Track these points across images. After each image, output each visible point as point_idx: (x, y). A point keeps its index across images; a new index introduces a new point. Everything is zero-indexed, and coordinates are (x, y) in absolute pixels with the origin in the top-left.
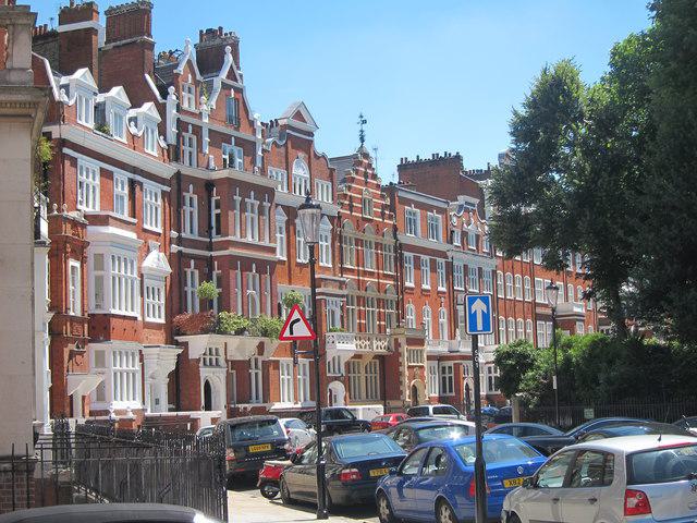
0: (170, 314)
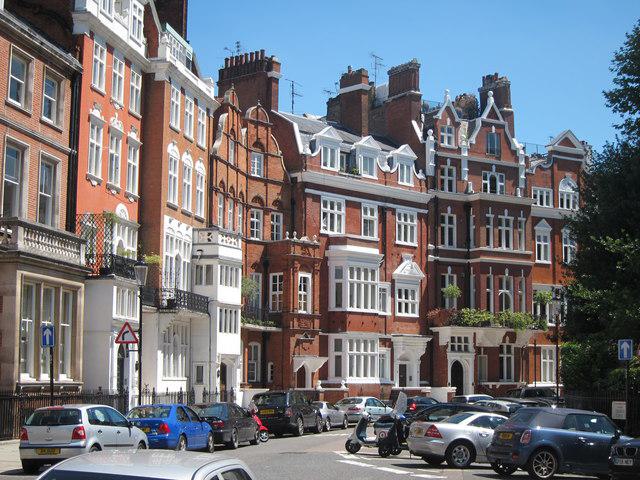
0: (425, 307)
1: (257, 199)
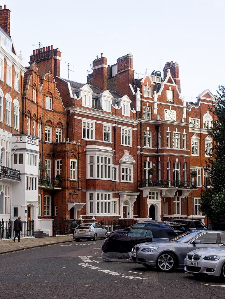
1: (49, 121)
